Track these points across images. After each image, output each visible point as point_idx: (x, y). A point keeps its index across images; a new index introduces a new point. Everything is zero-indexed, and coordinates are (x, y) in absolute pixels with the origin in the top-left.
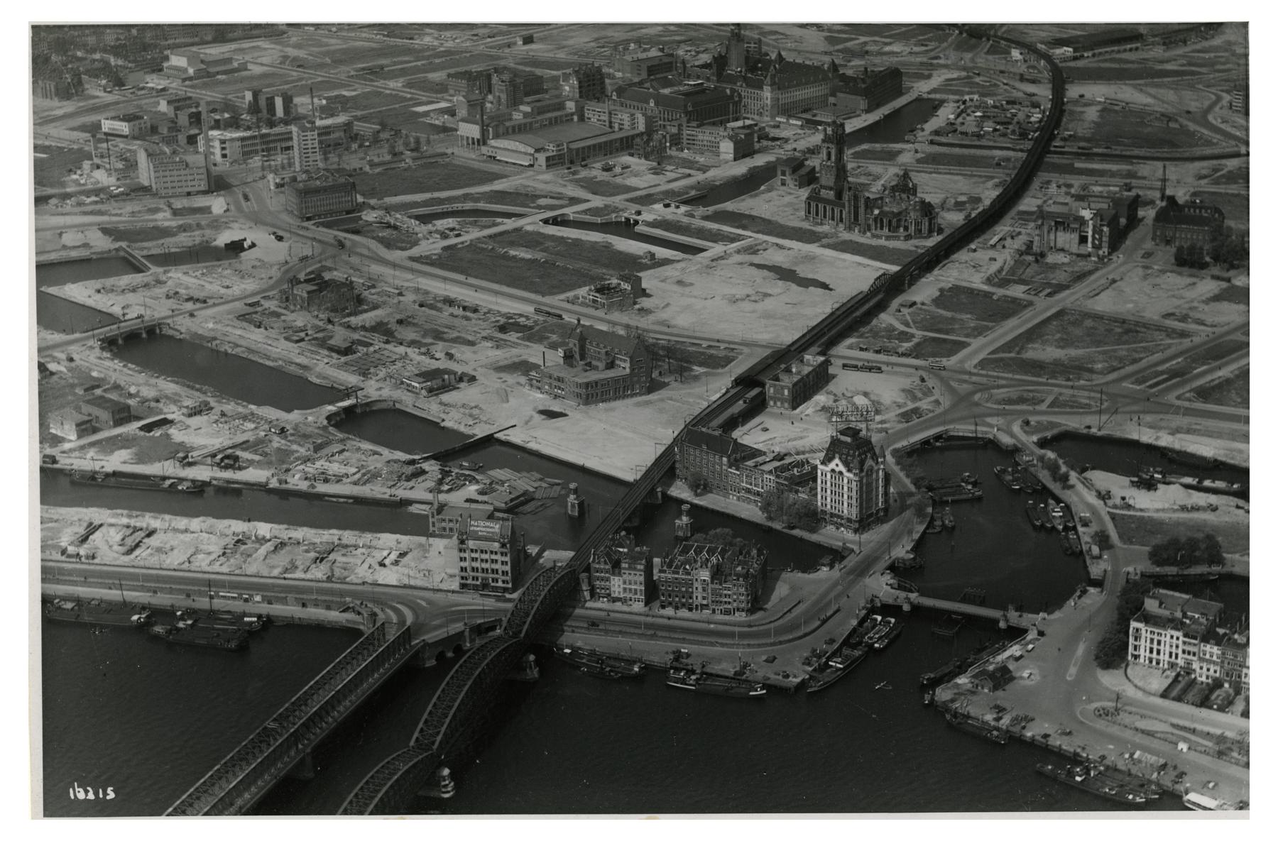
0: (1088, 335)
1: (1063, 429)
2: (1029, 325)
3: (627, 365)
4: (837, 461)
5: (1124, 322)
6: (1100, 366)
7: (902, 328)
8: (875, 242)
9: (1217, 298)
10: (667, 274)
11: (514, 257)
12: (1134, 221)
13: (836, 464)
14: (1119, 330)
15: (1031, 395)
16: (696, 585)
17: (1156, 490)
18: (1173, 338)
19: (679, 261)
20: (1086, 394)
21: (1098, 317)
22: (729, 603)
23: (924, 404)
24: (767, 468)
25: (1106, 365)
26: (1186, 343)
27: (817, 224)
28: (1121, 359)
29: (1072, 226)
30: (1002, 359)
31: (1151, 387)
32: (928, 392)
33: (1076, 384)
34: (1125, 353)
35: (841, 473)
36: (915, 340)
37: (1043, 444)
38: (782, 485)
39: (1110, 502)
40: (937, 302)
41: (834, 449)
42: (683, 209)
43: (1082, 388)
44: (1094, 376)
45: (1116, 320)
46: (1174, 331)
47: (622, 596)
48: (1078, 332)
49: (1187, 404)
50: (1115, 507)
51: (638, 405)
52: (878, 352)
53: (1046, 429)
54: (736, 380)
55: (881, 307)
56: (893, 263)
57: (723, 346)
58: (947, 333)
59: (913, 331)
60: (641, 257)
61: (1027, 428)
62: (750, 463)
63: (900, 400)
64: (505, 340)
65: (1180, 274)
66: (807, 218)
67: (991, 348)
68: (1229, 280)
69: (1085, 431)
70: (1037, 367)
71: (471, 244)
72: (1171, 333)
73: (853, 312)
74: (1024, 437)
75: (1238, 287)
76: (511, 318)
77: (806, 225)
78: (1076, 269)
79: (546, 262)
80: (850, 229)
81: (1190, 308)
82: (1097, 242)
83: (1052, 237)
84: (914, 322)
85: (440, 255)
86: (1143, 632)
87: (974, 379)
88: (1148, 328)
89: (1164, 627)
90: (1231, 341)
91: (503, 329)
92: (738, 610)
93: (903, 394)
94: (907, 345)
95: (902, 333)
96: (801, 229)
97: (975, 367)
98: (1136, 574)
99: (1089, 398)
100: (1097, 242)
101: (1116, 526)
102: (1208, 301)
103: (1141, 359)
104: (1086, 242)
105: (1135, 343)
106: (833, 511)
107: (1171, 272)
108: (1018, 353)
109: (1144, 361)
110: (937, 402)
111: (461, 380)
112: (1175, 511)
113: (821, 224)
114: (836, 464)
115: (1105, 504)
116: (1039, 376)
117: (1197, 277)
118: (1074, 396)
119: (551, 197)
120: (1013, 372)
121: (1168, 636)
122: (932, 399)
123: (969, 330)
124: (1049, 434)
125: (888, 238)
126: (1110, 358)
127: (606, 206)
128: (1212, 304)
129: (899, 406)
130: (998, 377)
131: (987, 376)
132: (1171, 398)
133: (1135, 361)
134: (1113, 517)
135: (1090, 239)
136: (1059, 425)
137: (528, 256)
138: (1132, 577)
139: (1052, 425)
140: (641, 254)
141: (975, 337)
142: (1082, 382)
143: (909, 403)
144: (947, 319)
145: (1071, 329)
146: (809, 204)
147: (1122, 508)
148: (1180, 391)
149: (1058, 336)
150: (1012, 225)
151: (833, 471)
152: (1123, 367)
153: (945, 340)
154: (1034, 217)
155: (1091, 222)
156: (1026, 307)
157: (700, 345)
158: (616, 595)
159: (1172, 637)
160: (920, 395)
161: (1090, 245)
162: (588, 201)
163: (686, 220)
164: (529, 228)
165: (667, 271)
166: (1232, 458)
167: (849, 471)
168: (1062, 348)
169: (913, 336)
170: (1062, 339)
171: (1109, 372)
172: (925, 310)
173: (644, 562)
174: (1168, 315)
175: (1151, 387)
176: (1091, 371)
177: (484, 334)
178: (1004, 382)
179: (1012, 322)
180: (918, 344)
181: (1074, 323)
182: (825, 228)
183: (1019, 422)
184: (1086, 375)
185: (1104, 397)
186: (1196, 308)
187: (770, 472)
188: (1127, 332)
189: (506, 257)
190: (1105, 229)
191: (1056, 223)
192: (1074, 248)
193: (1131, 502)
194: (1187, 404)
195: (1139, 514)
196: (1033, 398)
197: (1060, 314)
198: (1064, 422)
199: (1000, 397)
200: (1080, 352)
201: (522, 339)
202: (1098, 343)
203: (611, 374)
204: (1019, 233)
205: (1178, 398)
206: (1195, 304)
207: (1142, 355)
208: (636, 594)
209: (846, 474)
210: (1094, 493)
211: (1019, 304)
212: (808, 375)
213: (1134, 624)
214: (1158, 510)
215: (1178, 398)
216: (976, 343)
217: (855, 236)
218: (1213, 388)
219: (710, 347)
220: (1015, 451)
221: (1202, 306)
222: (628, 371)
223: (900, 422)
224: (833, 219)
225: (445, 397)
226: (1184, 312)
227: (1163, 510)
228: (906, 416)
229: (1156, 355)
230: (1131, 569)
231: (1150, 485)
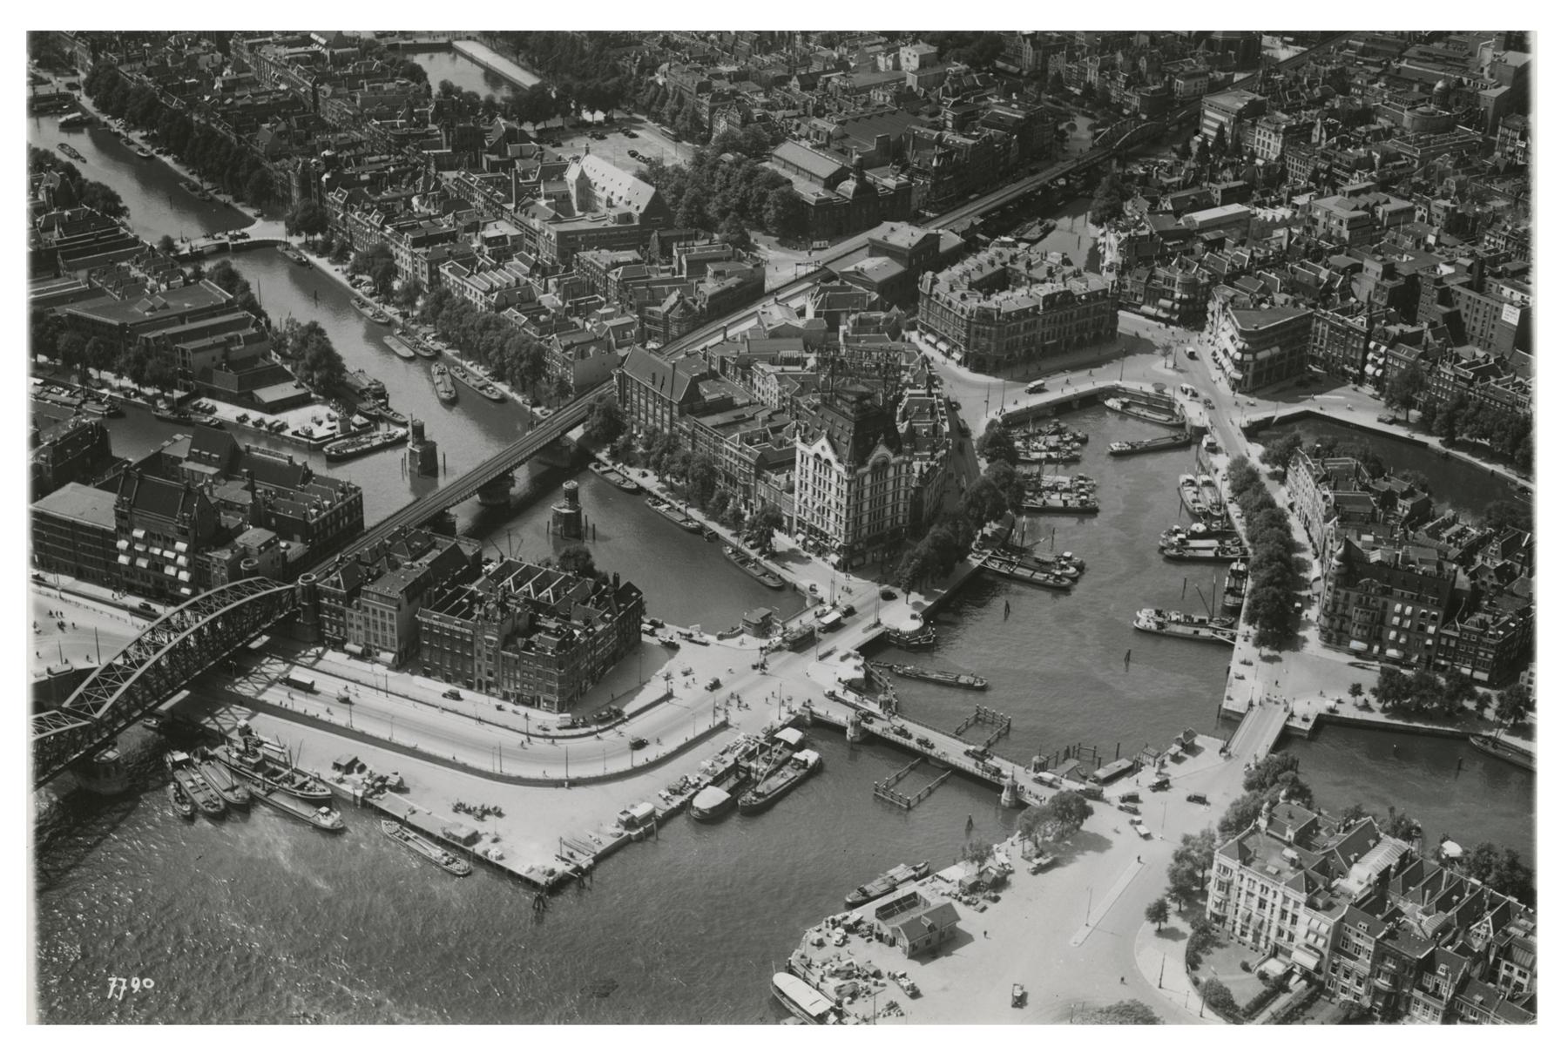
4: (823, 441)
13: (822, 447)
35: (828, 462)
106: (814, 523)
151: (817, 456)
167: (839, 461)
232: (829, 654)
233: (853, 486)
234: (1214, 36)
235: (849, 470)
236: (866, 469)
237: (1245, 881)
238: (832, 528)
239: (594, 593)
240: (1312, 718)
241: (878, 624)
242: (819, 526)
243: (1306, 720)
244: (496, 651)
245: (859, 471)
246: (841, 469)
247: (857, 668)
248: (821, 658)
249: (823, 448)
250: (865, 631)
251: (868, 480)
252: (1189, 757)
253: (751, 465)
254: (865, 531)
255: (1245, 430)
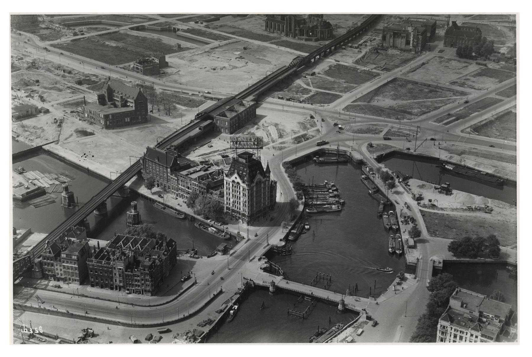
0: (409, 93)
1: (392, 150)
2: (376, 87)
3: (133, 105)
4: (236, 175)
5: (429, 86)
6: (416, 111)
7: (305, 86)
8: (299, 42)
9: (479, 74)
10: (185, 55)
11: (108, 45)
12: (433, 37)
13: (235, 177)
14: (427, 90)
15: (375, 127)
16: (114, 271)
17: (451, 194)
18: (457, 96)
19: (193, 49)
20: (407, 128)
21: (415, 83)
22: (139, 286)
23: (311, 132)
24: (194, 176)
25: (419, 110)
26: (465, 99)
27: (271, 32)
28: (428, 107)
29: (403, 35)
30: (359, 106)
31: (446, 124)
32: (313, 125)
33: (402, 121)
34: (430, 103)
35: (238, 183)
36: (312, 94)
37: (380, 159)
38: (202, 188)
39: (422, 202)
40: (327, 73)
41: (235, 165)
42: (205, 24)
43: (405, 124)
44: (413, 117)
45: (425, 85)
46: (457, 92)
47: (63, 277)
48: (403, 91)
49: (467, 136)
50: (425, 206)
51: (138, 129)
52: (288, 100)
53: (383, 149)
54: (198, 115)
55: (296, 75)
56: (306, 52)
57: (201, 94)
58: (329, 90)
59: (311, 88)
60: (173, 46)
61: (371, 149)
62: (184, 173)
63: (296, 129)
64: (79, 89)
65: (459, 61)
66: (266, 30)
67: (354, 99)
68: (485, 65)
69: (406, 152)
70: (379, 111)
71: (88, 39)
72: (456, 93)
73: (278, 77)
74: (368, 155)
75: (490, 69)
76: (88, 77)
77: (265, 33)
78: (403, 57)
79: (123, 48)
80: (287, 35)
81: (465, 79)
82: (415, 44)
83: (392, 41)
84: (312, 83)
85: (68, 44)
86: (449, 329)
87: (342, 117)
88: (442, 90)
89: (466, 326)
90: (490, 98)
91: (80, 83)
92: (145, 291)
93: (298, 125)
94: (306, 96)
95: (305, 89)
96: (262, 35)
97: (343, 110)
98: (440, 263)
99: (410, 130)
100: (415, 44)
101: (425, 221)
102: (474, 76)
103: (440, 107)
104: (409, 44)
105: (436, 98)
106: (234, 208)
107: (455, 60)
108: (369, 102)
109: (442, 108)
110: (318, 131)
111: (40, 112)
112: (464, 210)
113: (273, 33)
114: (235, 177)
115: (419, 204)
116: (380, 116)
117: (468, 63)
118: (400, 129)
119: (140, 18)
120: (365, 113)
121: (469, 335)
122: (315, 128)
123: (343, 89)
124: (383, 153)
125: (306, 40)
126: (422, 106)
127: (166, 22)
128: (478, 77)
129: (295, 133)
130: (356, 116)
131: (349, 115)
132: (458, 131)
133: (436, 108)
134: (422, 213)
135: (411, 42)
136: (392, 147)
137: (114, 45)
138: (437, 264)
139: (387, 147)
140: (173, 44)
141: (345, 92)
142: (405, 120)
143: (301, 130)
144: (331, 82)
145: (399, 89)
146: (268, 22)
147: (429, 207)
148: (463, 127)
149: (392, 93)
150: (371, 35)
151: (233, 181)
152: (430, 112)
153: (328, 94)
154: (507, 320)
155: (412, 33)
156: (375, 76)
157: (188, 93)
158: (59, 276)
159: (472, 335)
160: (309, 126)
161: (411, 45)
162: (158, 20)
163: (204, 29)
164: (122, 32)
165: (186, 54)
166: (498, 173)
167: (244, 182)
168: (394, 99)
169: (310, 91)
170: (395, 95)
171: (421, 115)
172: (320, 77)
173: (77, 253)
174: (453, 83)
175: (446, 124)
176: (410, 113)
177: (70, 85)
178: (359, 119)
179: (368, 84)
180: (313, 96)
181: (401, 86)
182: (275, 35)
183: (366, 144)
184: (408, 116)
185: (419, 130)
186: (468, 79)
187: (195, 180)
188: (431, 91)
189: (103, 45)
190: (420, 37)
191: (394, 33)
192: (403, 46)
193: (435, 203)
194: (467, 136)
195: (440, 212)
196: (375, 130)
197: (394, 80)
198: (393, 145)
199: (356, 129)
200: (405, 102)
201: (89, 88)
202: (415, 97)
203: (124, 110)
204: (375, 39)
205: (462, 131)
206: (468, 77)
207: (440, 105)
208: (73, 276)
209: (242, 184)
210: (411, 196)
211: (372, 75)
212: (241, 113)
213: (441, 323)
214: (453, 210)
215: (462, 131)
216: (346, 96)
217: (290, 39)
218: (483, 126)
219: (193, 95)
220: (361, 163)
221: (473, 79)
222: (134, 108)
223: (294, 143)
224: (279, 30)
225: (26, 122)
226: (463, 81)
227: (456, 209)
228: (298, 140)
229: (448, 105)
230: (435, 258)
231: (448, 191)
232: (254, 258)
233: (250, 191)
234: (324, 18)
235: (248, 185)
236: (254, 184)
237: (453, 330)
238: (242, 209)
239: (157, 244)
240: (441, 261)
241: (268, 245)
242: (236, 209)
243: (440, 263)
244: (123, 272)
245: (252, 185)
246: (245, 186)
247: (266, 263)
248: (251, 261)
249: (236, 178)
250: (264, 248)
251: (255, 189)
252: (403, 282)
253: (205, 189)
254: (255, 209)
255: (375, 159)
